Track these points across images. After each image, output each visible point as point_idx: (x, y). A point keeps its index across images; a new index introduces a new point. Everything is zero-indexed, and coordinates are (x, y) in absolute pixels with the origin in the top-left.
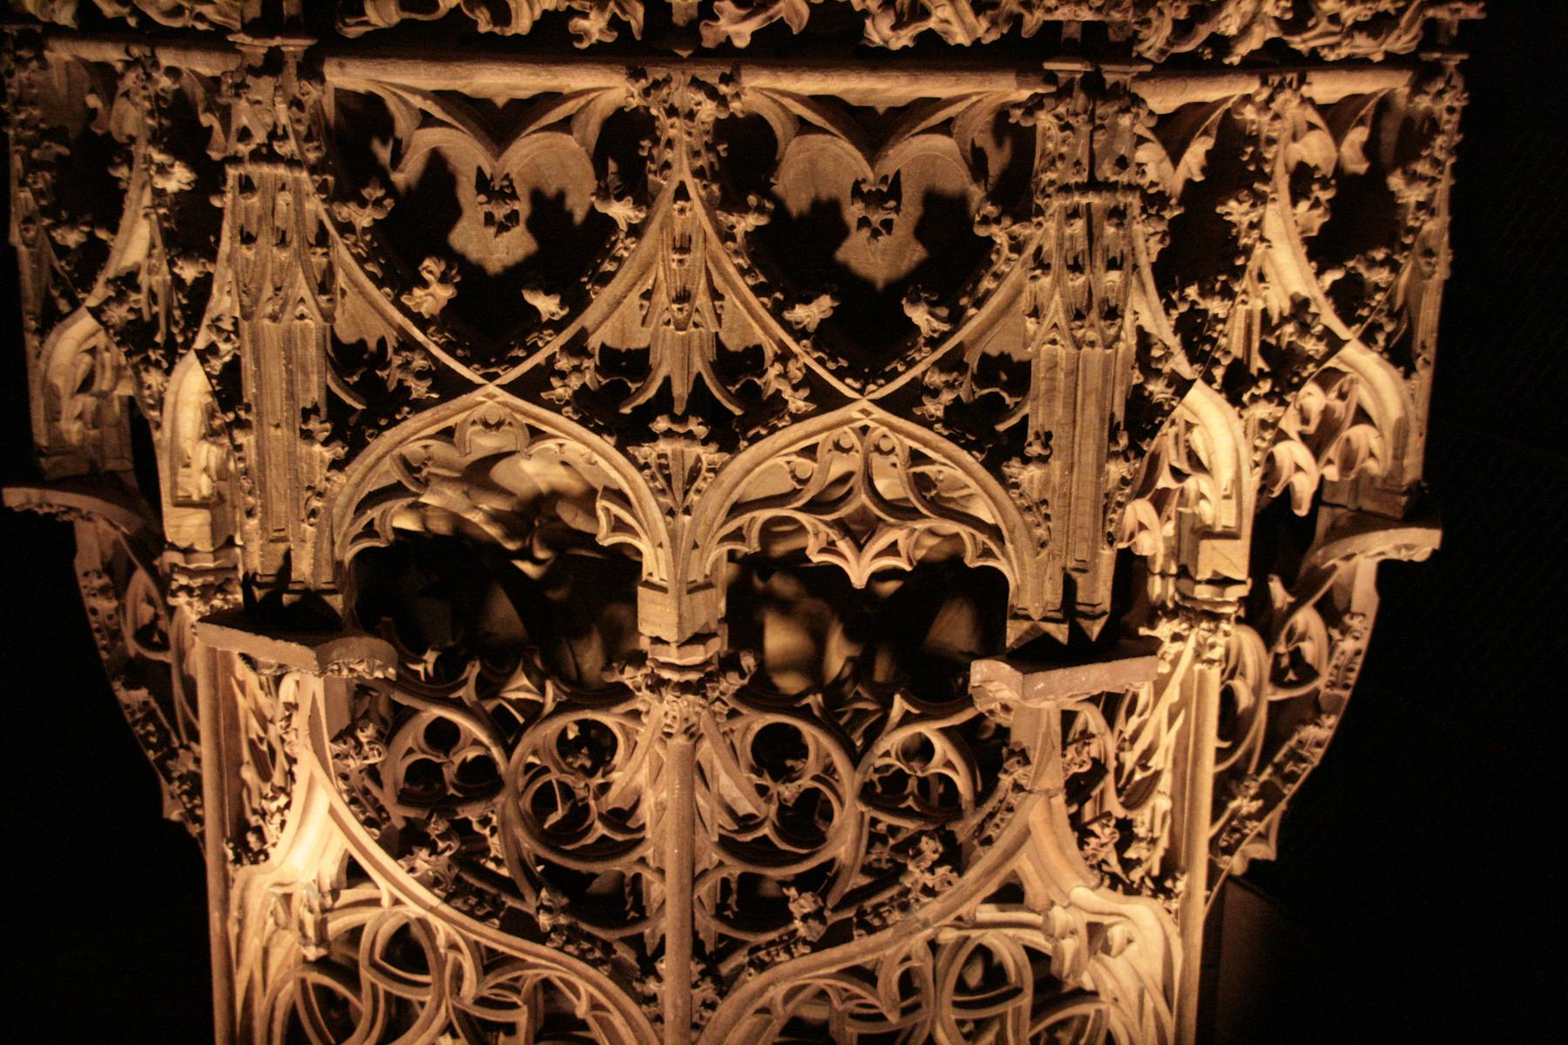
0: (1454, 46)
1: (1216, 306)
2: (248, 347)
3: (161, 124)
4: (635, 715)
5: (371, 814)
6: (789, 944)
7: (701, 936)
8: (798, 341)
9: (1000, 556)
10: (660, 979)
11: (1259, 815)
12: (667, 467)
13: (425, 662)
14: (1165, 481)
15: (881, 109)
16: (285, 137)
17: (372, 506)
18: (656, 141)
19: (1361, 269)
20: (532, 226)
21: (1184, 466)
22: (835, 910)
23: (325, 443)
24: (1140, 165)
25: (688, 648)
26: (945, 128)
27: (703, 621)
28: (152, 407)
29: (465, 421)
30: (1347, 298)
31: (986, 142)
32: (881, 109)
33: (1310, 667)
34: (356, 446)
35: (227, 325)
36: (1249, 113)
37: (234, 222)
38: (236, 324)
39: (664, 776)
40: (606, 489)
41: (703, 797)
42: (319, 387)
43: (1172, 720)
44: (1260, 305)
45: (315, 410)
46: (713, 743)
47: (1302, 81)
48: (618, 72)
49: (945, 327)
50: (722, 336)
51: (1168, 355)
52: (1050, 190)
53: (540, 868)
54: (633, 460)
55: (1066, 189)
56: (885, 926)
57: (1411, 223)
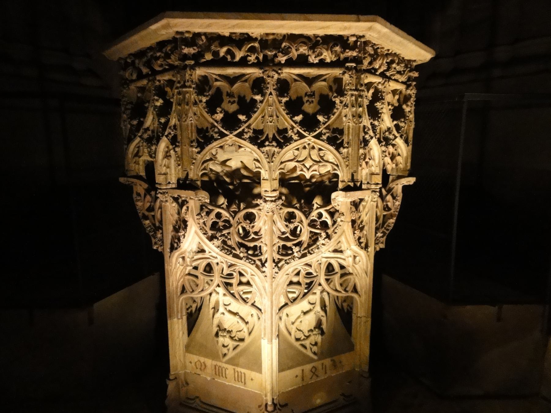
0: (413, 81)
6: (293, 258)
7: (274, 258)
8: (296, 124)
9: (338, 170)
10: (266, 267)
11: (382, 237)
12: (268, 153)
18: (265, 83)
22: (303, 251)
23: (196, 148)
25: (273, 192)
26: (325, 80)
27: (275, 187)
34: (202, 148)
39: (267, 222)
41: (275, 228)
43: (366, 215)
45: (194, 141)
46: (277, 214)
49: (326, 120)
50: (278, 126)
51: (369, 130)
52: (347, 90)
54: (261, 151)
55: (351, 90)
56: (314, 253)
57: (408, 115)
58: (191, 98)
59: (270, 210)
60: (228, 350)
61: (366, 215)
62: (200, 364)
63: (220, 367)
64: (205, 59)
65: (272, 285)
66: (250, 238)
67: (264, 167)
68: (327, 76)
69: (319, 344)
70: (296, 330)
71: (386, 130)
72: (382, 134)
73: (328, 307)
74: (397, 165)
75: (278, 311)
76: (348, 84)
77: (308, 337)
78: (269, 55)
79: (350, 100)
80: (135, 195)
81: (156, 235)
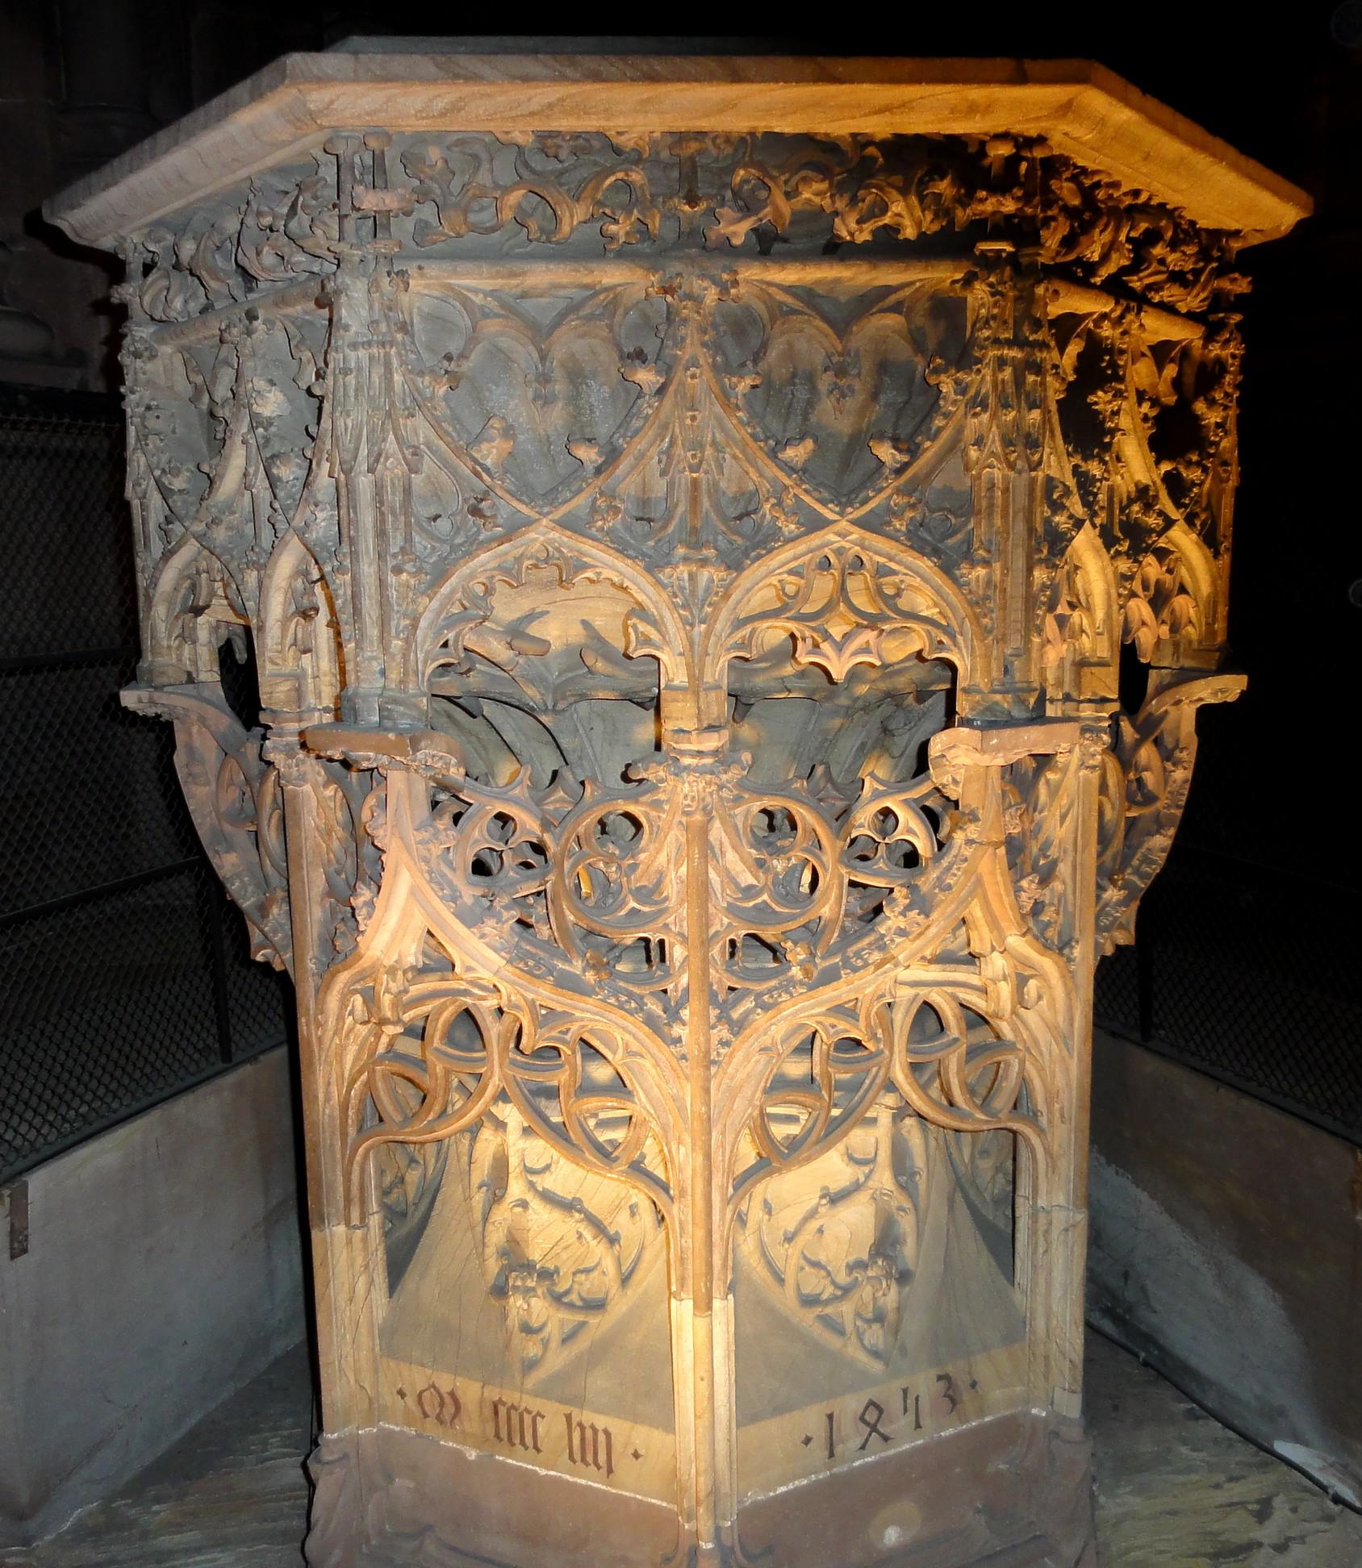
6: (788, 986)
26: (896, 308)
27: (714, 716)
48: (641, 267)
49: (905, 458)
54: (659, 582)
55: (997, 342)
56: (866, 965)
60: (546, 1343)
61: (1063, 818)
62: (437, 1401)
63: (513, 1407)
68: (907, 292)
70: (803, 1263)
73: (924, 1175)
74: (1175, 628)
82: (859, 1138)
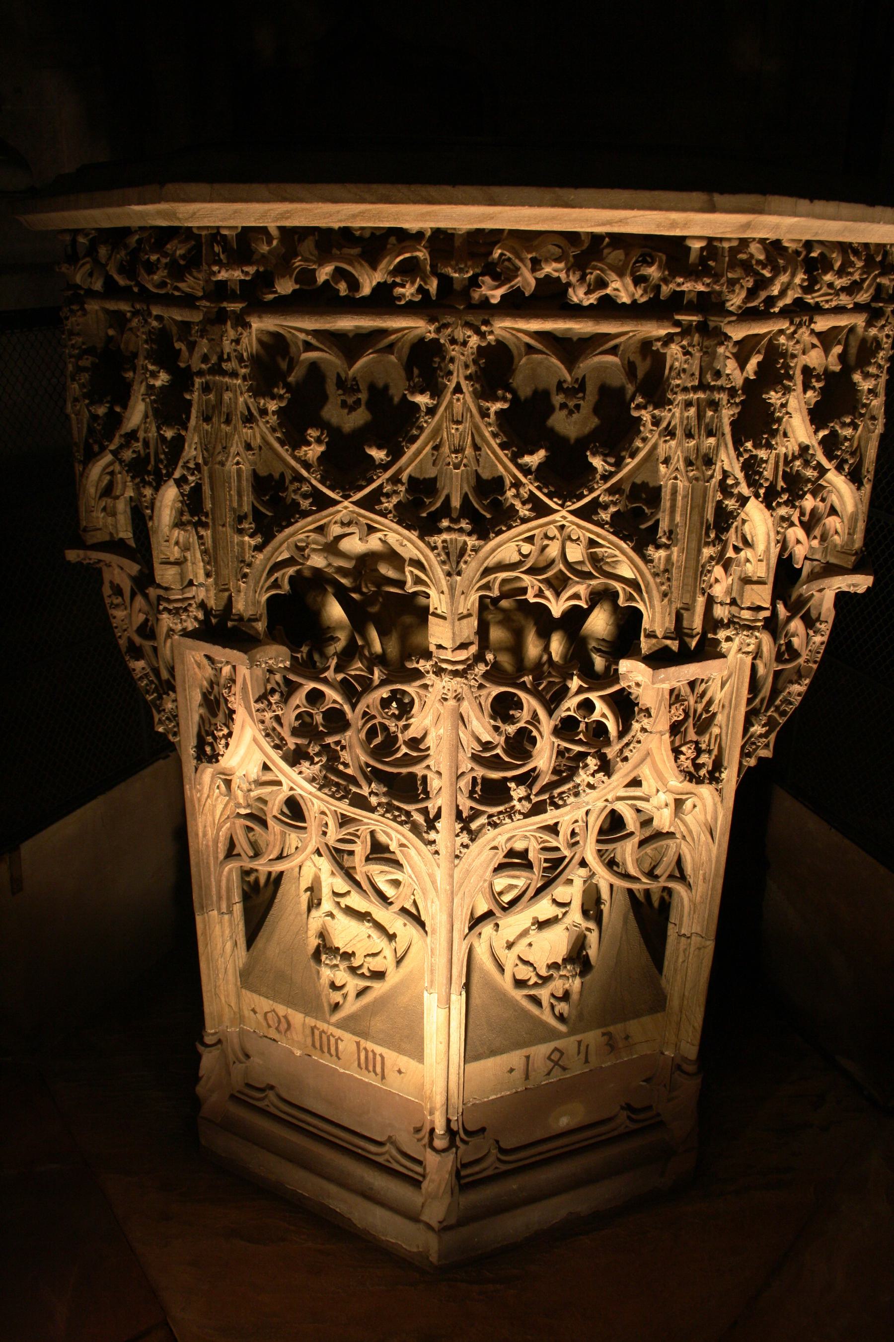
1: (762, 454)
2: (207, 480)
3: (151, 347)
4: (425, 687)
5: (277, 742)
6: (510, 813)
7: (461, 808)
8: (526, 476)
10: (438, 832)
11: (766, 735)
13: (302, 652)
14: (730, 553)
15: (575, 339)
16: (229, 359)
17: (276, 572)
18: (443, 358)
19: (837, 428)
20: (370, 406)
21: (741, 545)
22: (536, 795)
23: (251, 536)
24: (728, 375)
25: (458, 651)
26: (614, 351)
28: (147, 508)
29: (330, 522)
30: (830, 445)
31: (637, 359)
32: (575, 339)
33: (796, 651)
34: (268, 538)
35: (192, 465)
36: (782, 340)
37: (199, 408)
38: (197, 465)
40: (411, 559)
42: (248, 504)
44: (784, 450)
46: (470, 703)
47: (811, 321)
49: (613, 469)
50: (480, 471)
51: (737, 484)
52: (675, 390)
53: (369, 769)
54: (428, 544)
55: (685, 390)
56: (565, 805)
58: (236, 403)
59: (450, 695)
60: (345, 996)
61: (723, 685)
62: (276, 1019)
63: (323, 1031)
64: (276, 292)
65: (452, 876)
66: (399, 755)
67: (437, 584)
68: (622, 339)
69: (575, 996)
70: (518, 962)
71: (796, 453)
72: (781, 464)
73: (608, 904)
74: (824, 538)
75: (467, 931)
76: (679, 374)
77: (546, 980)
78: (457, 278)
79: (681, 418)
80: (107, 590)
81: (161, 705)
82: (561, 892)
